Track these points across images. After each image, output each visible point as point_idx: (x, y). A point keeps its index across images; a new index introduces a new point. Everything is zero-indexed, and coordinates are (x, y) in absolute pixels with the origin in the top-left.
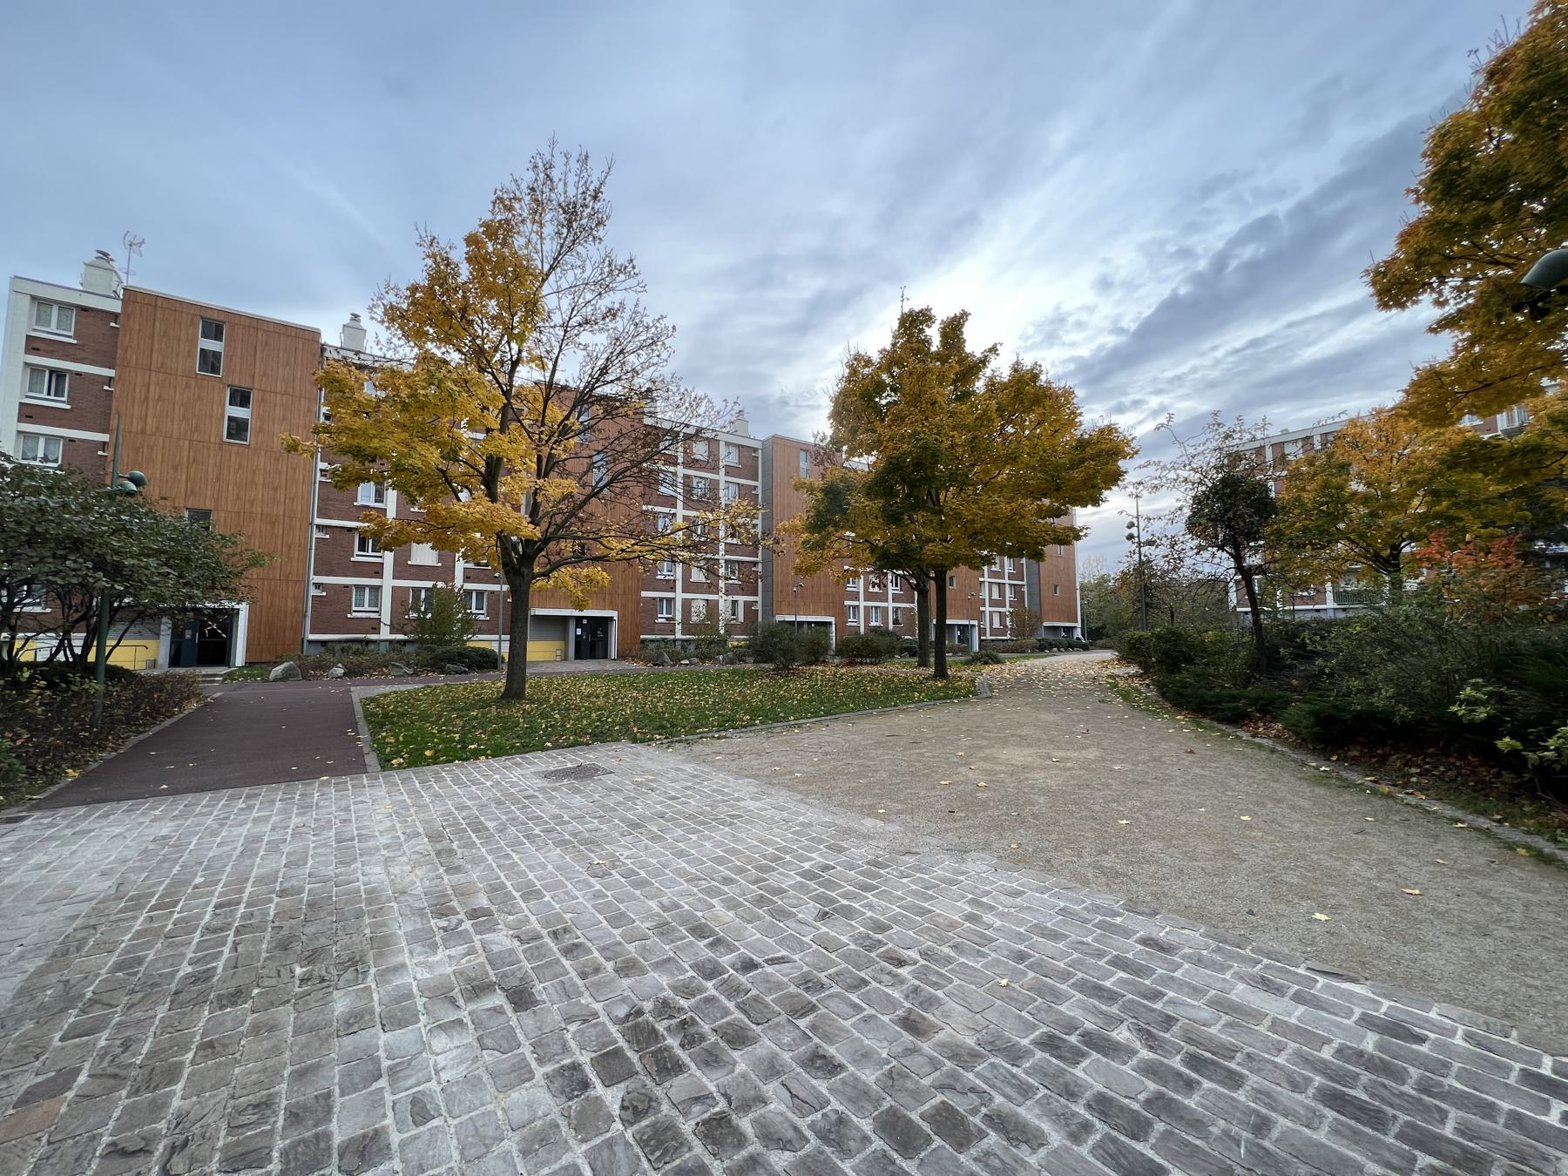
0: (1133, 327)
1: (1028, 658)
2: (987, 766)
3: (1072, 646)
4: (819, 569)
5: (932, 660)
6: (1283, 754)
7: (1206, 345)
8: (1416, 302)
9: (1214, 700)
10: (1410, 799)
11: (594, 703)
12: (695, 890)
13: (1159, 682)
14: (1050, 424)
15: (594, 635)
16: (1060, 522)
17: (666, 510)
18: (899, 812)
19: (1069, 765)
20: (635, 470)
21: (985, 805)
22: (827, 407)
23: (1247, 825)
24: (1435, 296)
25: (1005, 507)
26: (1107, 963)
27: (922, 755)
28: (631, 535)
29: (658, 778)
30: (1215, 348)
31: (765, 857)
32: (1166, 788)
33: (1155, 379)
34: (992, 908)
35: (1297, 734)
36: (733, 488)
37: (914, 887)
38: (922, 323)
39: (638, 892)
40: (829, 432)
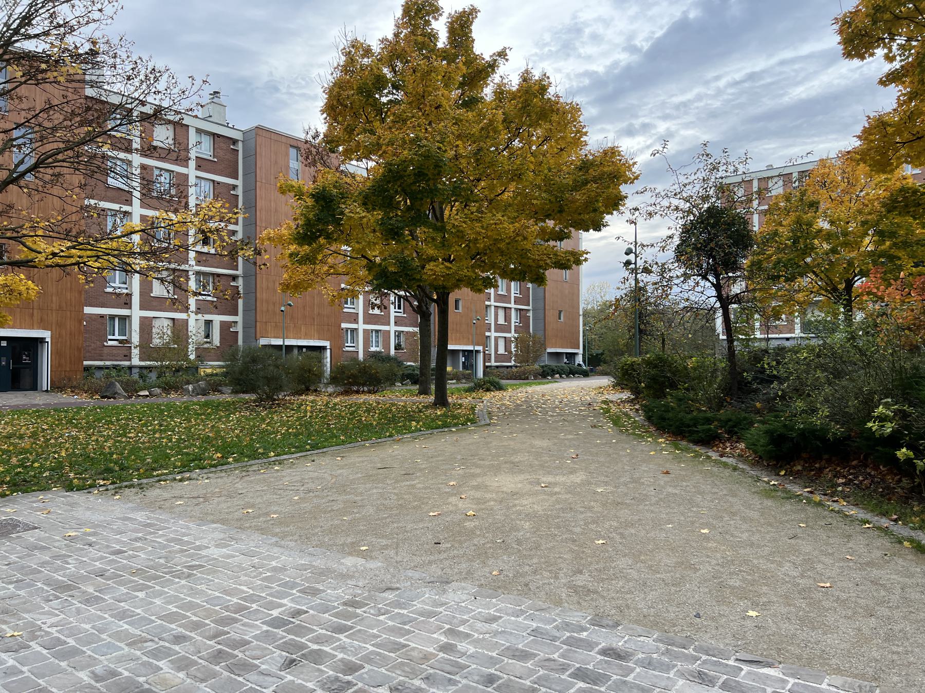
0: (646, 46)
1: (530, 385)
2: (478, 494)
3: (573, 372)
4: (310, 286)
5: (433, 387)
6: (743, 471)
7: (710, 75)
8: (872, 55)
9: (691, 423)
10: (836, 507)
11: (15, 445)
12: (138, 653)
13: (646, 406)
14: (556, 141)
15: (17, 360)
16: (564, 246)
17: (116, 207)
18: (386, 547)
19: (557, 489)
20: (70, 153)
21: (471, 533)
22: (321, 100)
23: (706, 538)
24: (886, 51)
25: (509, 228)
26: (570, 676)
27: (413, 486)
28: (67, 235)
29: (99, 530)
30: (717, 78)
31: (227, 608)
32: (641, 507)
33: (663, 104)
34: (468, 636)
35: (755, 452)
36: (207, 187)
37: (390, 623)
38: (428, 14)
39: (64, 664)
40: (323, 128)
